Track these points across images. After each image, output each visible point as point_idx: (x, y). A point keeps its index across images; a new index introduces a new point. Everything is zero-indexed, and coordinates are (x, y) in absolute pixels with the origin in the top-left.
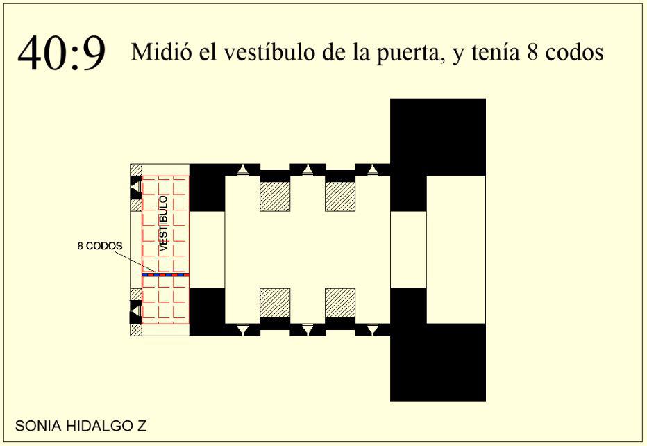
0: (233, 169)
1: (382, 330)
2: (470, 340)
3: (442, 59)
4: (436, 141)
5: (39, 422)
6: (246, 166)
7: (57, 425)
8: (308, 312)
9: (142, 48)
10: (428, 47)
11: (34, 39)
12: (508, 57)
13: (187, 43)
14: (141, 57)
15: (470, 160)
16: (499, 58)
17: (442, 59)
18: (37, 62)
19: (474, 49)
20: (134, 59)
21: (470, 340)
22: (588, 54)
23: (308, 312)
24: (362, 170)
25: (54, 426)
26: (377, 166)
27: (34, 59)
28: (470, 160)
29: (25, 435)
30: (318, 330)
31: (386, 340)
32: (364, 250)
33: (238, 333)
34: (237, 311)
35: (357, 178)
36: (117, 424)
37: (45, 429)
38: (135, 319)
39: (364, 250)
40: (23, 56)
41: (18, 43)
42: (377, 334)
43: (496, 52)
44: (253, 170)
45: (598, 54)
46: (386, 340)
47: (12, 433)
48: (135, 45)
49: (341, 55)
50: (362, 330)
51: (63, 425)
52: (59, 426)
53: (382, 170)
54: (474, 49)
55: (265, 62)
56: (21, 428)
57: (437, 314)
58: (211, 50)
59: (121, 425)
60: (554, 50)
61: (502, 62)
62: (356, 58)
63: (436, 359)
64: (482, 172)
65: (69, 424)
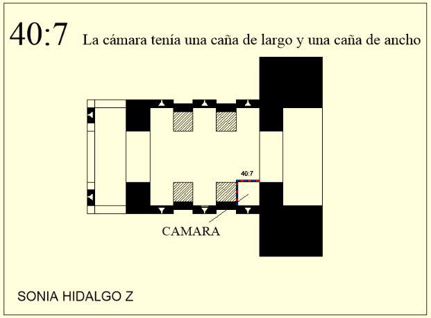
0: (155, 104)
1: (254, 210)
2: (313, 215)
5: (38, 292)
7: (55, 296)
8: (204, 197)
9: (186, 230)
11: (20, 25)
15: (311, 96)
18: (23, 40)
19: (153, 38)
21: (313, 215)
23: (204, 197)
24: (241, 103)
25: (52, 297)
26: (251, 101)
27: (21, 38)
28: (311, 96)
29: (27, 307)
30: (212, 210)
31: (256, 217)
32: (237, 154)
34: (159, 197)
36: (107, 294)
37: (44, 300)
38: (91, 203)
39: (237, 154)
41: (11, 27)
42: (251, 212)
44: (169, 104)
45: (59, 44)
46: (256, 217)
47: (14, 306)
48: (183, 228)
49: (377, 42)
50: (241, 210)
51: (60, 296)
52: (56, 297)
53: (254, 104)
54: (153, 38)
55: (319, 37)
57: (289, 199)
58: (406, 38)
59: (111, 295)
62: (263, 44)
63: (290, 229)
64: (321, 106)
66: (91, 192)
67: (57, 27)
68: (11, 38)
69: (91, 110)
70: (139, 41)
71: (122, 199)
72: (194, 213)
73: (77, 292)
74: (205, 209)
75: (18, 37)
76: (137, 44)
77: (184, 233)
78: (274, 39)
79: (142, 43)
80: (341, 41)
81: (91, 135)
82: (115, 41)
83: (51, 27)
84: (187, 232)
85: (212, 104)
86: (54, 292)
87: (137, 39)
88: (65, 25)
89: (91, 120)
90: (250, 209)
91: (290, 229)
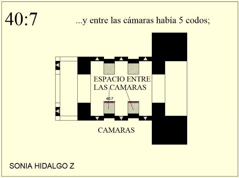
0: (94, 59)
1: (149, 118)
2: (181, 122)
3: (209, 23)
4: (169, 48)
5: (21, 164)
6: (98, 58)
7: (30, 166)
9: (112, 129)
10: (172, 19)
11: (11, 14)
12: (161, 22)
13: (130, 17)
14: (111, 132)
15: (181, 56)
16: (135, 23)
17: (209, 23)
18: (12, 22)
20: (95, 85)
21: (181, 122)
22: (201, 21)
24: (141, 59)
25: (29, 166)
27: (11, 21)
28: (181, 56)
29: (15, 172)
30: (125, 118)
31: (150, 122)
33: (96, 120)
35: (115, 62)
36: (59, 165)
37: (24, 168)
38: (58, 114)
40: (7, 20)
41: (6, 15)
42: (147, 120)
43: (96, 20)
44: (101, 59)
45: (33, 25)
46: (150, 122)
47: (8, 171)
48: (110, 128)
49: (106, 21)
50: (141, 118)
51: (33, 166)
52: (31, 166)
53: (149, 59)
56: (13, 167)
57: (169, 112)
59: (62, 165)
60: (189, 20)
61: (136, 24)
62: (112, 23)
63: (169, 129)
65: (36, 165)
66: (57, 108)
67: (32, 15)
68: (6, 21)
69: (57, 62)
70: (146, 21)
71: (76, 113)
72: (115, 120)
73: (43, 164)
74: (145, 118)
75: (10, 20)
76: (144, 23)
77: (110, 131)
78: (144, 20)
79: (147, 22)
80: (128, 21)
81: (58, 76)
82: (130, 21)
83: (28, 15)
84: (112, 130)
85: (125, 59)
86: (30, 164)
87: (144, 20)
88: (36, 14)
89: (58, 68)
90: (146, 117)
91: (169, 129)
